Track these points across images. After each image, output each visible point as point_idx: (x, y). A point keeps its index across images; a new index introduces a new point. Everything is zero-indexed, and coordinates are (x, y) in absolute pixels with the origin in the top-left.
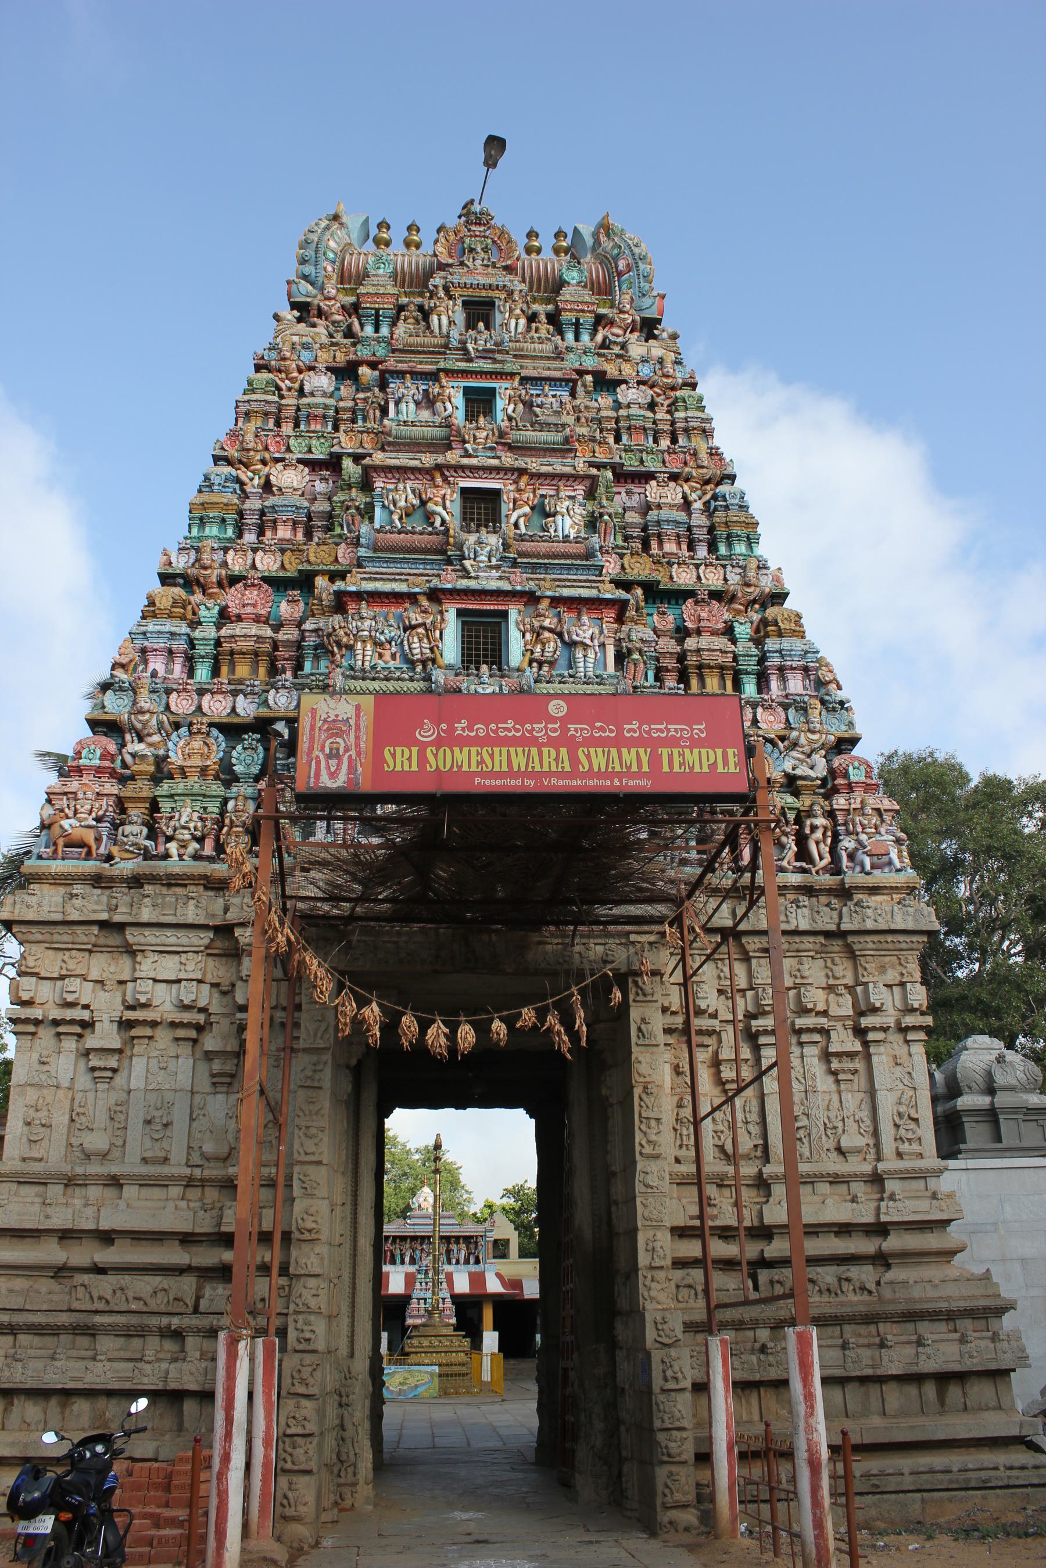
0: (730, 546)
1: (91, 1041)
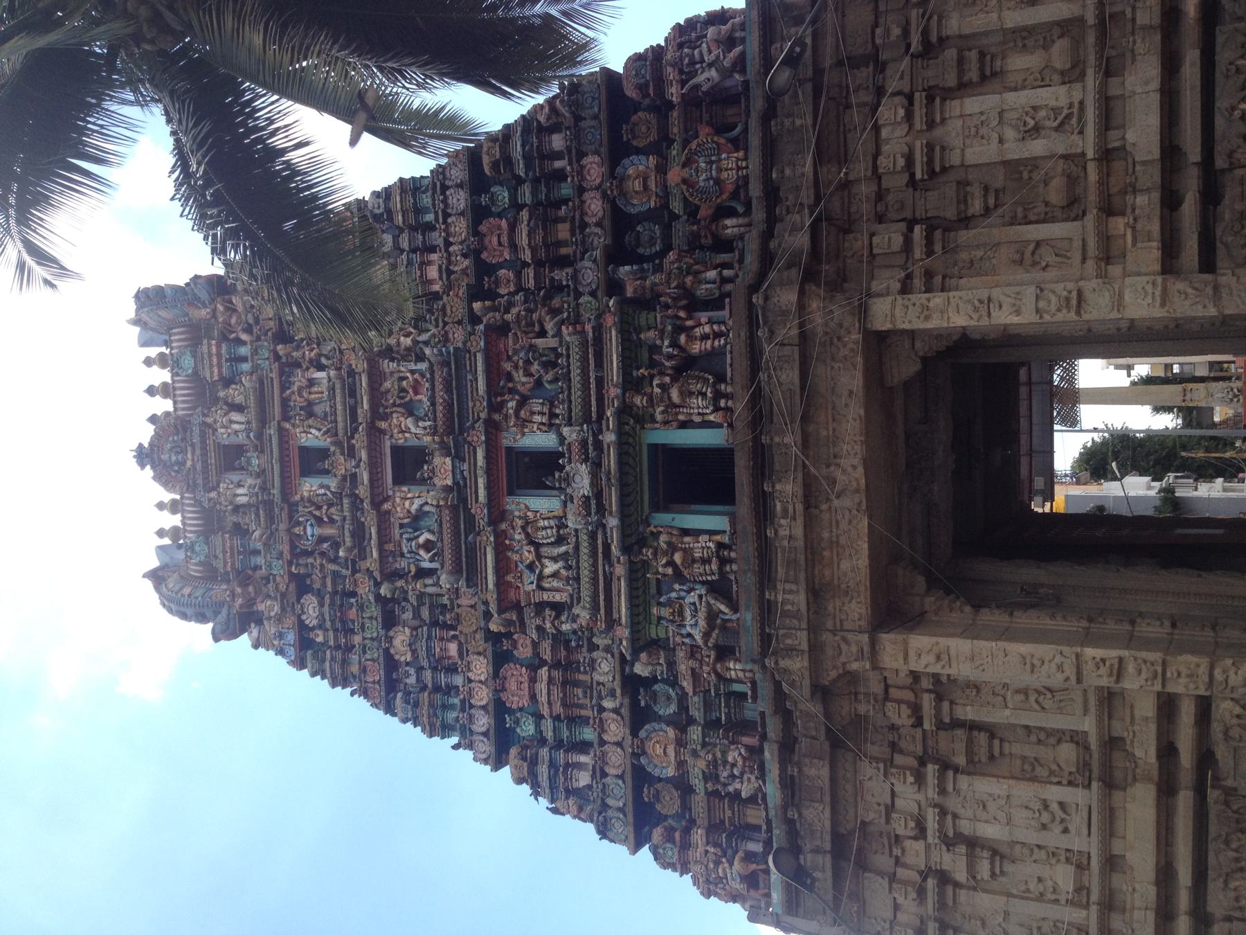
0: (425, 211)
1: (961, 876)
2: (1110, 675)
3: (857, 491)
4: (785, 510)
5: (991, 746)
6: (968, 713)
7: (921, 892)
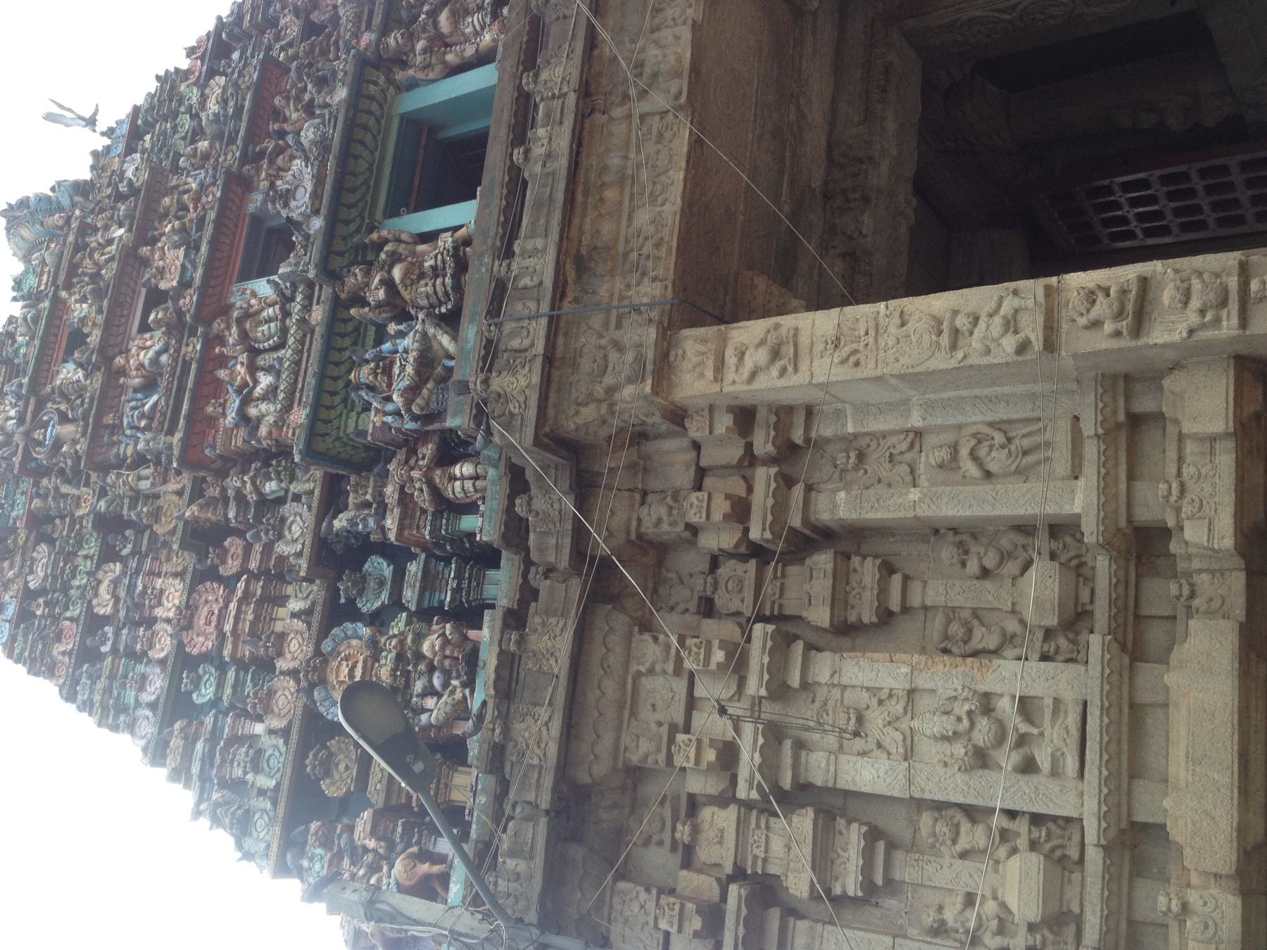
1: (799, 884)
2: (1119, 315)
3: (677, 74)
4: (548, 115)
5: (883, 591)
6: (839, 505)
7: (713, 917)
